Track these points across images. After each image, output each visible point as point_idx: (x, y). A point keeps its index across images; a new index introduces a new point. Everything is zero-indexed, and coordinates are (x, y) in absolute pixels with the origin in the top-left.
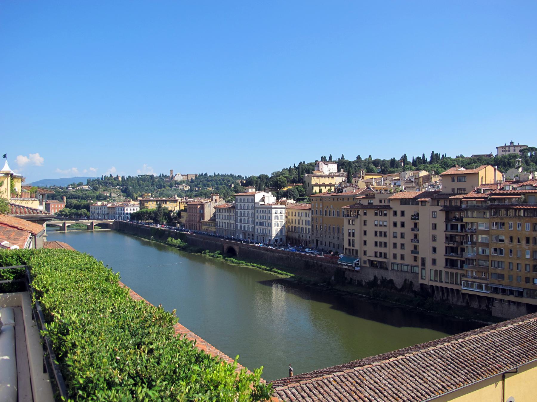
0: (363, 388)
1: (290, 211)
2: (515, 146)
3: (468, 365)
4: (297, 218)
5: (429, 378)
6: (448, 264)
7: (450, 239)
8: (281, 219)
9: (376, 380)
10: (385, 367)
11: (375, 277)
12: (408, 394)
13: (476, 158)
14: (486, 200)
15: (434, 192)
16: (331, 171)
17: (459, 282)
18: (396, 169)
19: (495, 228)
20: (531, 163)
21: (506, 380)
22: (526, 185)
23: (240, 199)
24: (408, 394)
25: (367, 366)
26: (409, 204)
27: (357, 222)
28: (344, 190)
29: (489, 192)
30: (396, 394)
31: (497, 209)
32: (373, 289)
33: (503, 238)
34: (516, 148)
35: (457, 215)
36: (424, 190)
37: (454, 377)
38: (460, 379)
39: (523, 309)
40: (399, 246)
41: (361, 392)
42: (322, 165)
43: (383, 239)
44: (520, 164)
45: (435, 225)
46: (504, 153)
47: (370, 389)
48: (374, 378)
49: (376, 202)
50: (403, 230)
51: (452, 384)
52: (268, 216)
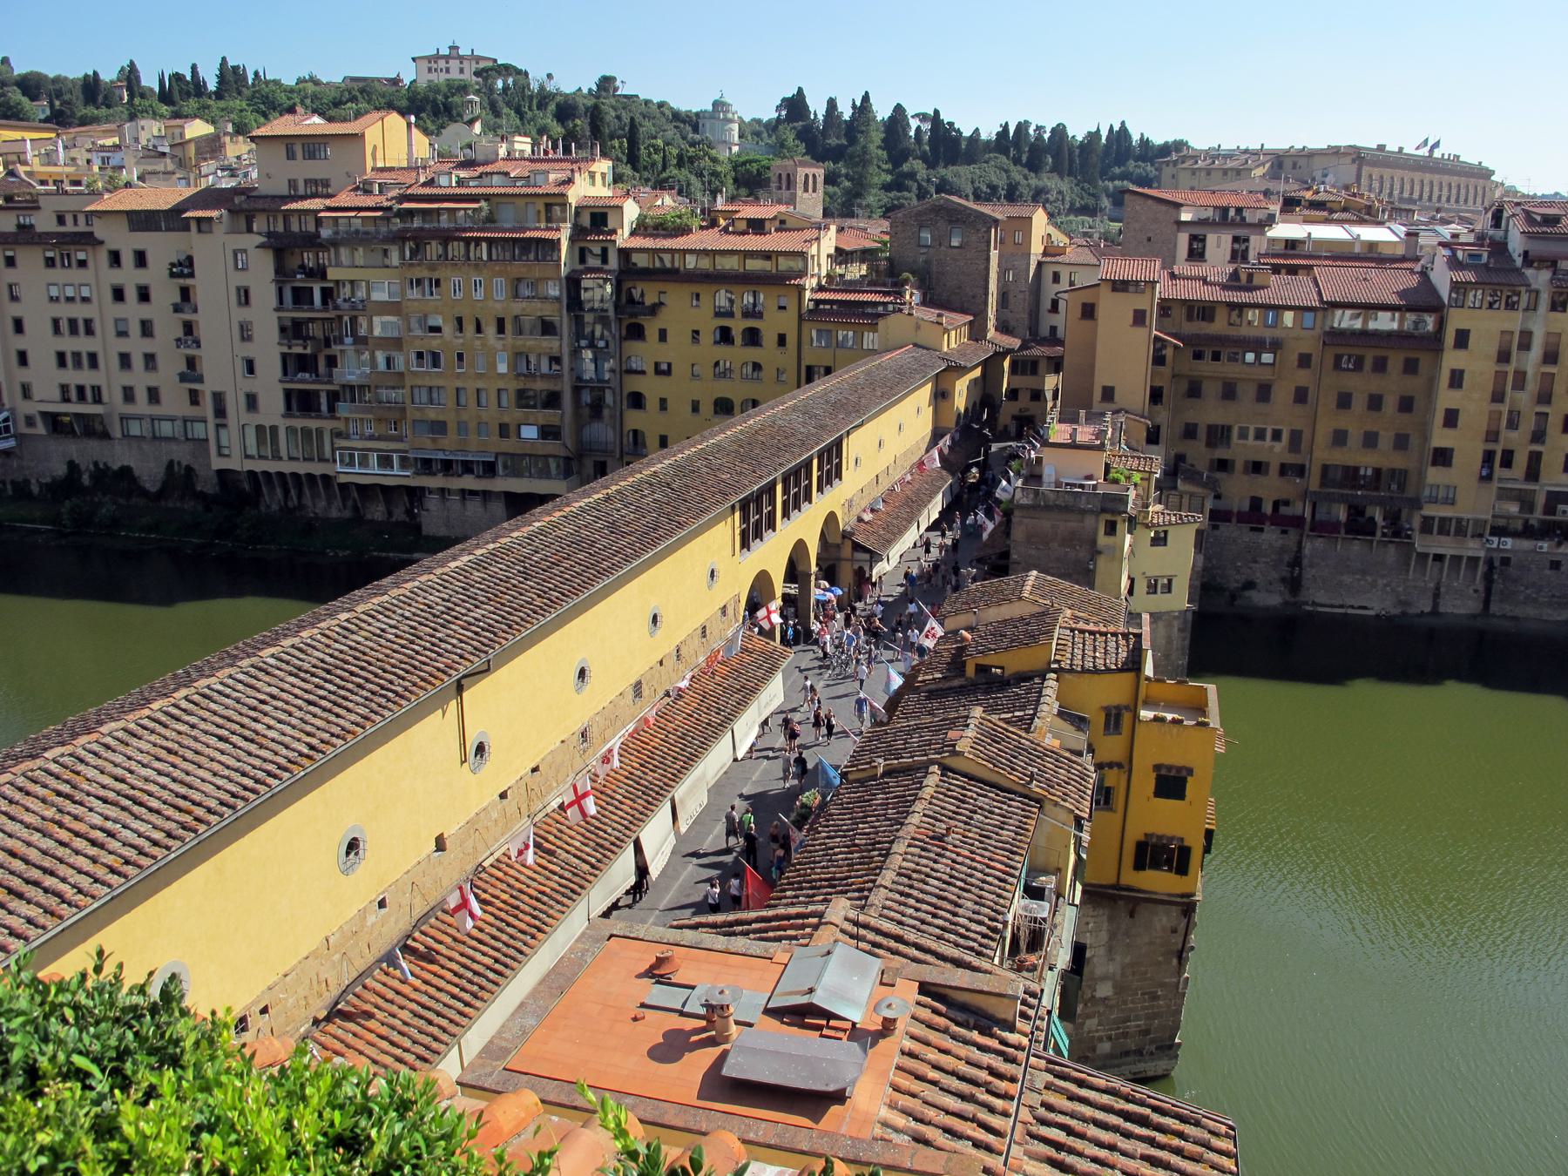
0: (81, 804)
2: (461, 58)
3: (370, 676)
5: (272, 734)
6: (294, 406)
7: (292, 330)
9: (119, 772)
10: (140, 731)
11: (72, 466)
12: (219, 788)
13: (356, 86)
14: (389, 214)
15: (234, 191)
17: (328, 454)
18: (103, 111)
19: (414, 294)
20: (506, 110)
21: (465, 695)
22: (492, 174)
24: (219, 788)
25: (83, 740)
26: (158, 229)
29: (394, 193)
30: (185, 798)
31: (418, 240)
32: (67, 503)
33: (437, 321)
34: (466, 64)
35: (309, 259)
36: (203, 184)
37: (338, 716)
38: (353, 717)
39: (498, 508)
40: (138, 362)
41: (76, 818)
43: (83, 344)
44: (478, 111)
45: (247, 292)
46: (433, 76)
47: (105, 801)
48: (109, 768)
49: (44, 222)
50: (145, 311)
51: (333, 735)
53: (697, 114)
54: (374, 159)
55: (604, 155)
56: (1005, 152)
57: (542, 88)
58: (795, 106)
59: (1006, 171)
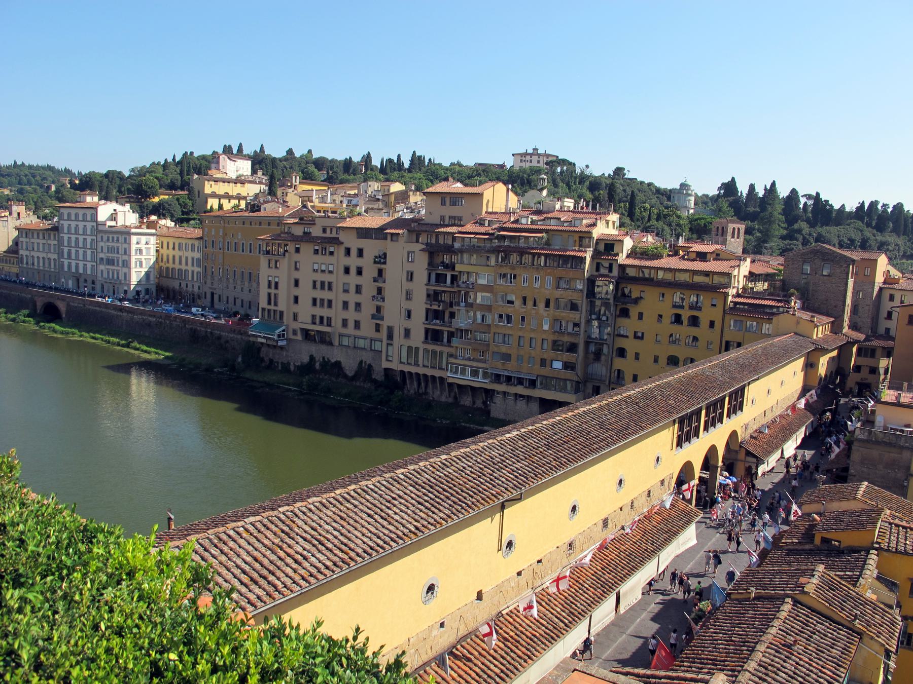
1: (165, 240)
2: (539, 155)
4: (177, 253)
8: (148, 253)
16: (240, 173)
23: (69, 215)
27: (284, 263)
28: (263, 207)
29: (496, 226)
35: (446, 259)
42: (223, 159)
46: (523, 164)
52: (122, 247)
53: (670, 190)
54: (487, 207)
55: (615, 211)
56: (862, 219)
57: (582, 172)
58: (729, 188)
59: (861, 231)
